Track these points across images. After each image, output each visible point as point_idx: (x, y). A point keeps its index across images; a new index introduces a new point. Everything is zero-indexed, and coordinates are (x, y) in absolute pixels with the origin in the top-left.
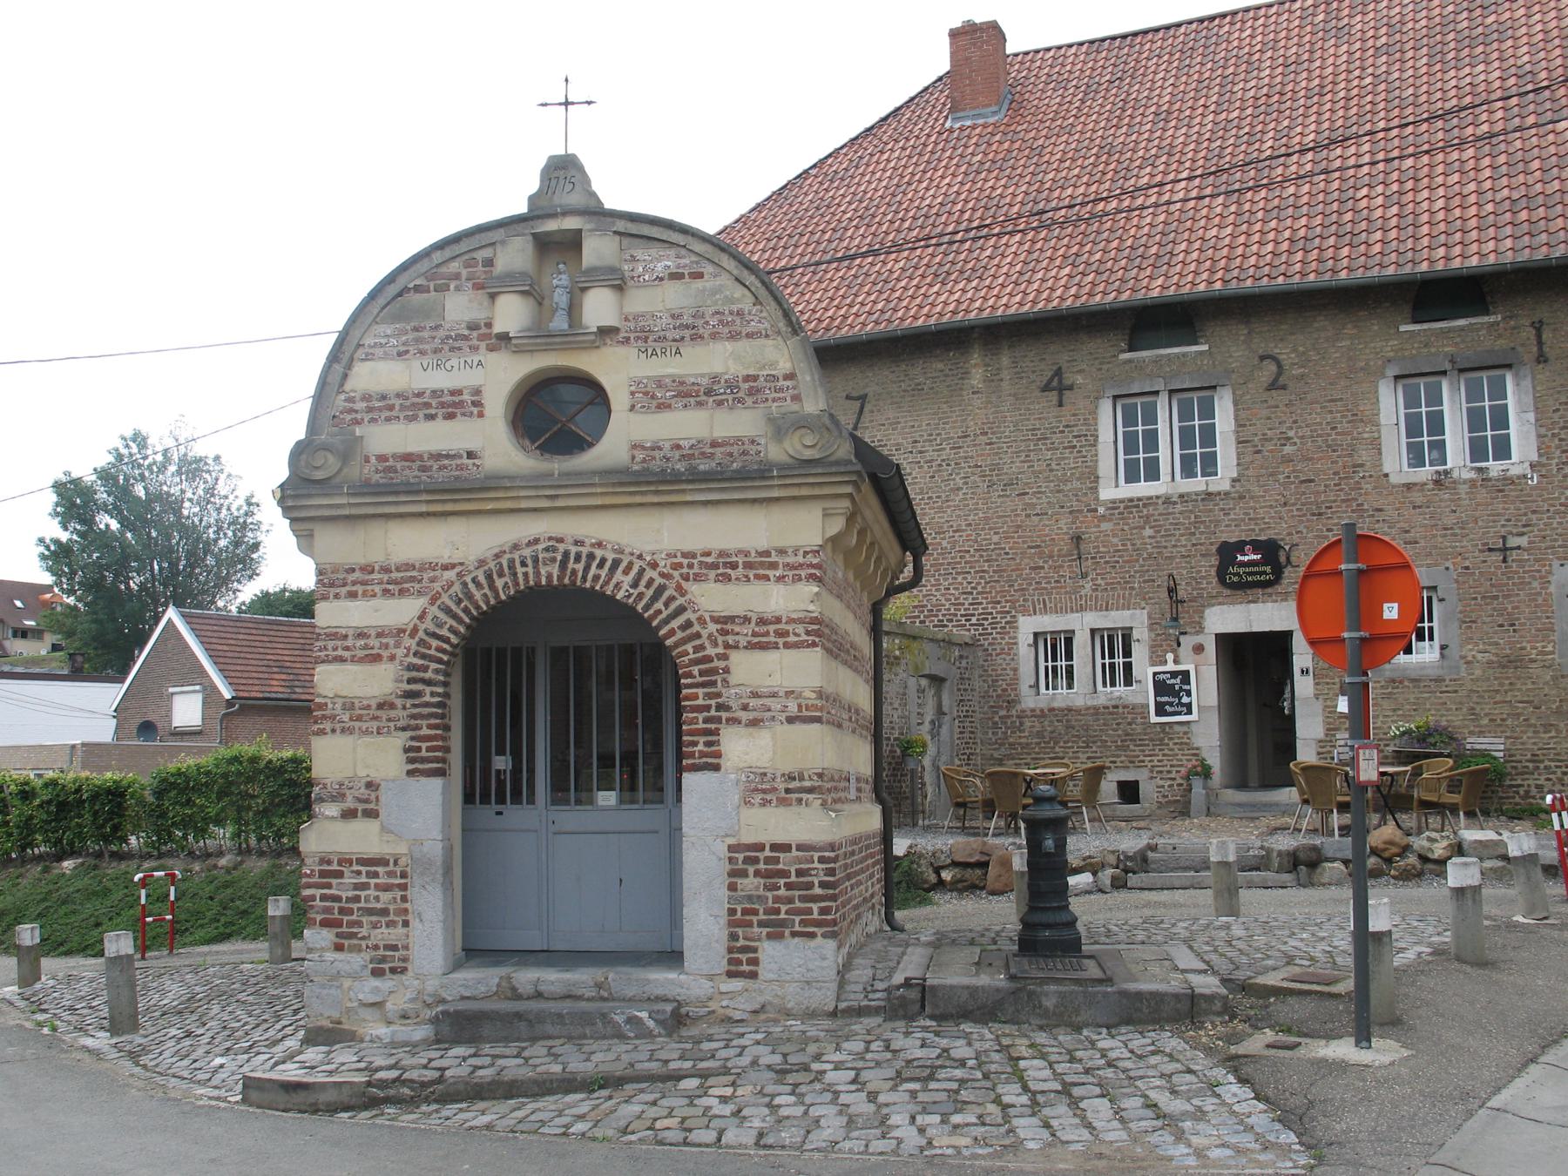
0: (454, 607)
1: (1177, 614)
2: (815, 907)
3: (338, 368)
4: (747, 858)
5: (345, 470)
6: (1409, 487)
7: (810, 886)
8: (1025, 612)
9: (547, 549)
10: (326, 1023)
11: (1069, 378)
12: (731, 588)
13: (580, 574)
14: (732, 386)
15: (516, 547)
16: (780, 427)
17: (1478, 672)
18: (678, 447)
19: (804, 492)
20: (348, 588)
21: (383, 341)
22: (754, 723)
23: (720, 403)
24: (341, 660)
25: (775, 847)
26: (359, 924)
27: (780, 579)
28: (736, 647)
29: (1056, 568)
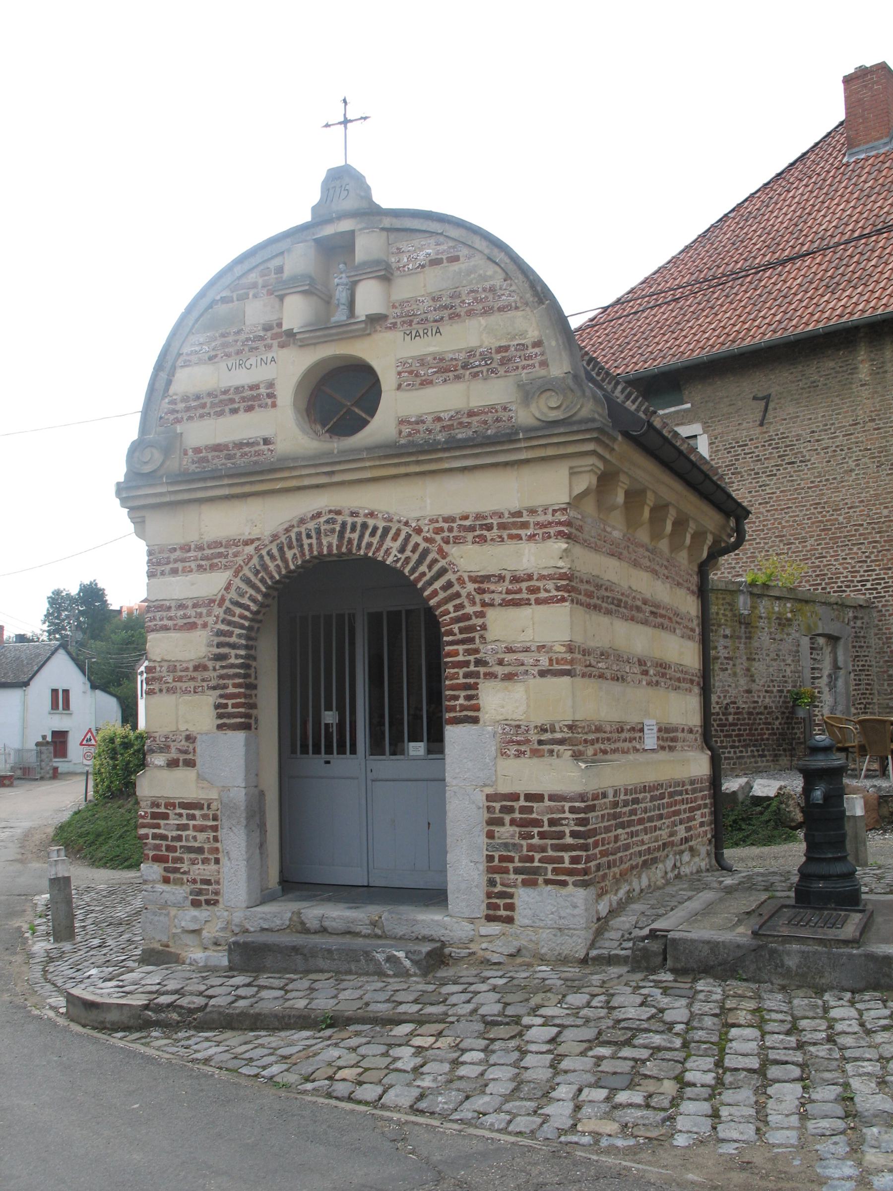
0: (253, 578)
2: (566, 856)
5: (168, 463)
9: (327, 522)
14: (486, 357)
15: (302, 521)
16: (529, 392)
18: (439, 419)
19: (550, 452)
20: (171, 566)
21: (197, 348)
22: (509, 677)
23: (475, 375)
25: (529, 797)
27: (531, 537)
28: (492, 605)
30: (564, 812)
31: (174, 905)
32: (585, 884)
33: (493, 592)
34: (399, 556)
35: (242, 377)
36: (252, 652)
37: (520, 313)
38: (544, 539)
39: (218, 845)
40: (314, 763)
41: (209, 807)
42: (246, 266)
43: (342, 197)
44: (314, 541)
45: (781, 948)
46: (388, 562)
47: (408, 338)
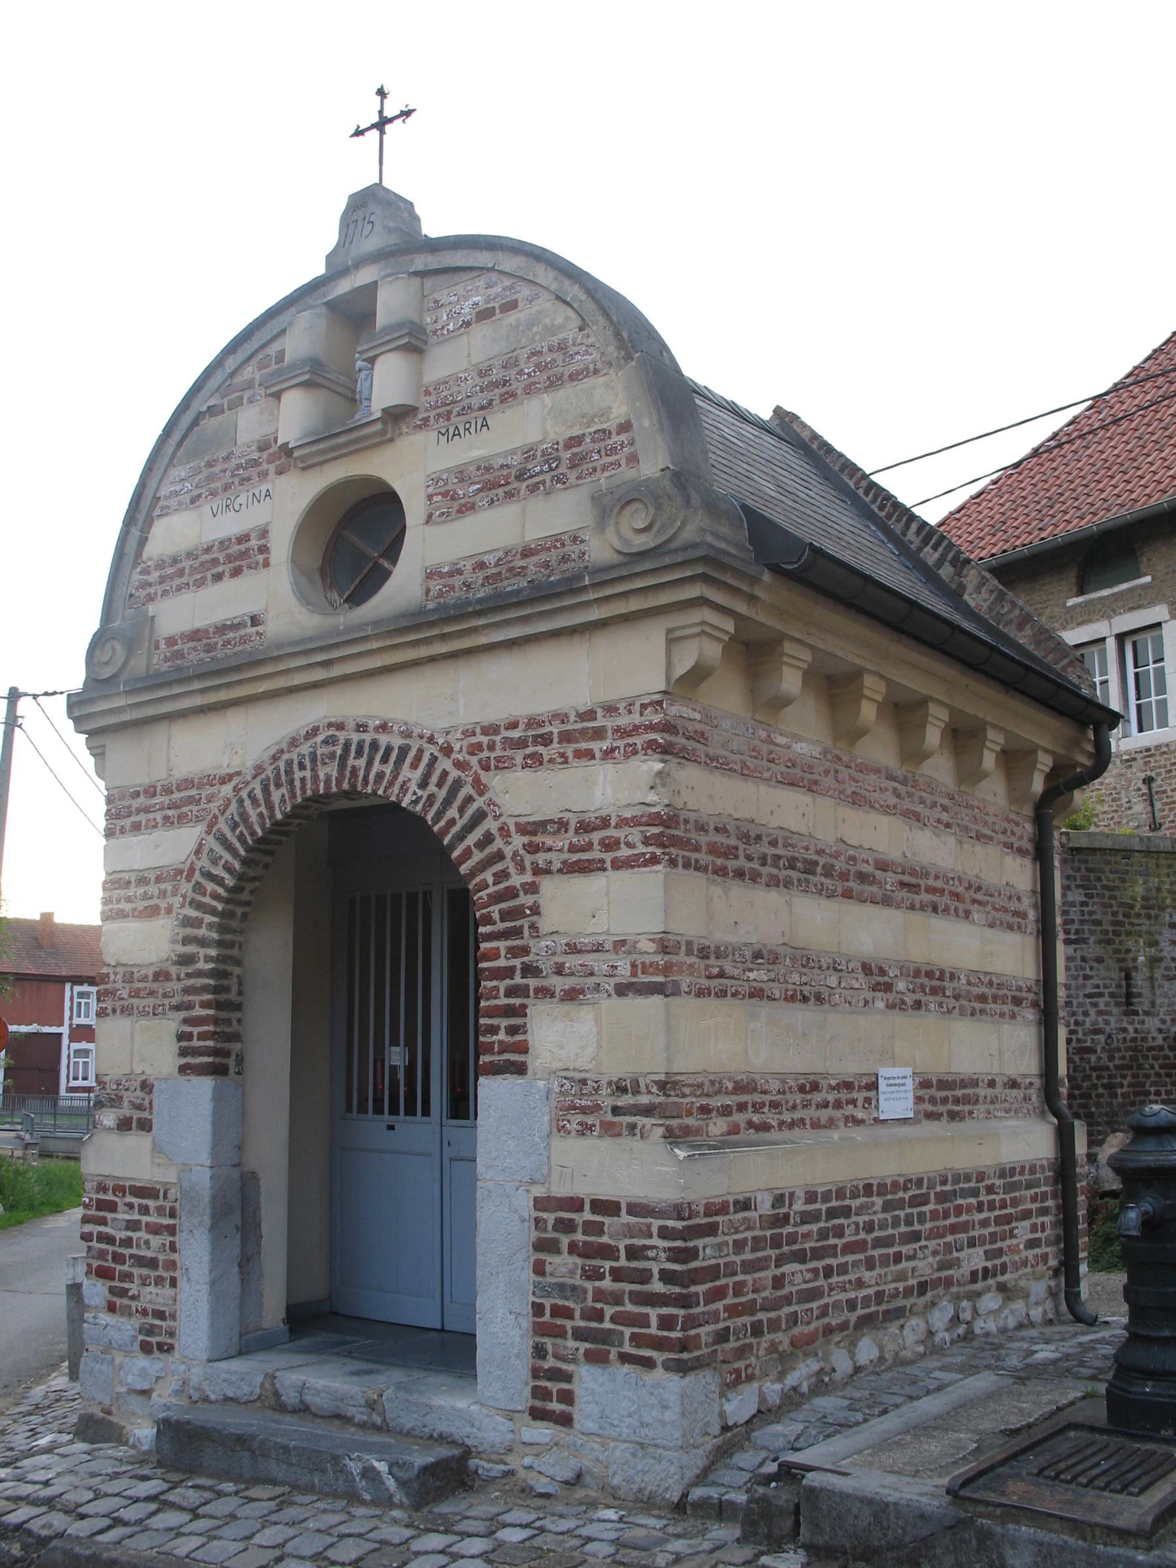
0: (229, 835)
2: (653, 1313)
3: (135, 532)
5: (132, 663)
9: (326, 742)
12: (545, 777)
13: (361, 774)
14: (551, 458)
15: (294, 743)
16: (608, 507)
18: (481, 565)
19: (634, 605)
20: (133, 819)
21: (178, 488)
22: (571, 995)
23: (533, 489)
25: (600, 1206)
27: (608, 754)
28: (548, 872)
30: (650, 1236)
31: (120, 1348)
32: (683, 1368)
33: (550, 849)
34: (420, 793)
35: (229, 525)
36: (234, 952)
37: (600, 380)
38: (627, 756)
39: (175, 1257)
40: (372, 1129)
41: (165, 1197)
42: (240, 356)
43: (365, 233)
44: (308, 774)
45: (999, 1530)
46: (404, 805)
47: (443, 439)
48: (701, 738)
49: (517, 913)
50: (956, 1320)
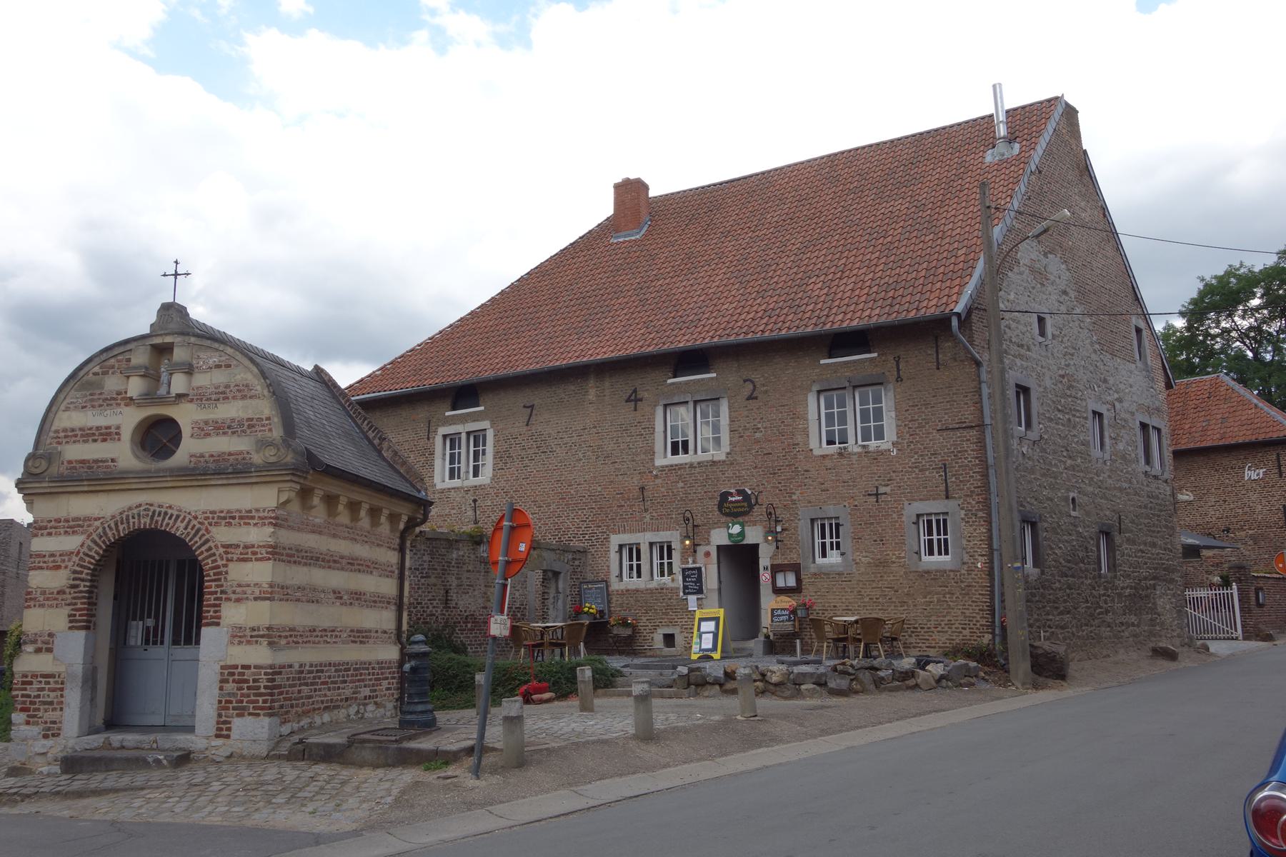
1: (695, 532)
2: (260, 699)
4: (230, 673)
6: (824, 457)
7: (259, 688)
8: (614, 532)
10: (18, 765)
11: (641, 394)
12: (232, 530)
14: (241, 424)
15: (130, 509)
16: (263, 444)
17: (863, 570)
22: (238, 600)
23: (233, 433)
24: (41, 568)
25: (244, 667)
26: (38, 710)
27: (255, 525)
29: (631, 506)
32: (271, 715)
48: (286, 520)
49: (220, 573)
50: (358, 712)
